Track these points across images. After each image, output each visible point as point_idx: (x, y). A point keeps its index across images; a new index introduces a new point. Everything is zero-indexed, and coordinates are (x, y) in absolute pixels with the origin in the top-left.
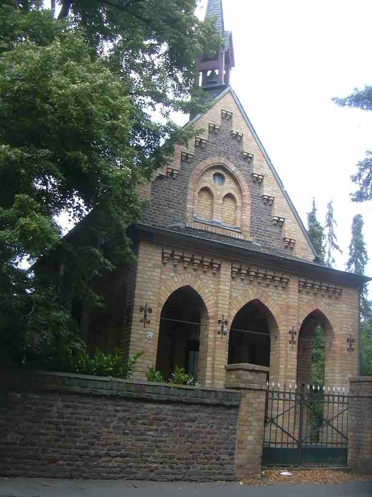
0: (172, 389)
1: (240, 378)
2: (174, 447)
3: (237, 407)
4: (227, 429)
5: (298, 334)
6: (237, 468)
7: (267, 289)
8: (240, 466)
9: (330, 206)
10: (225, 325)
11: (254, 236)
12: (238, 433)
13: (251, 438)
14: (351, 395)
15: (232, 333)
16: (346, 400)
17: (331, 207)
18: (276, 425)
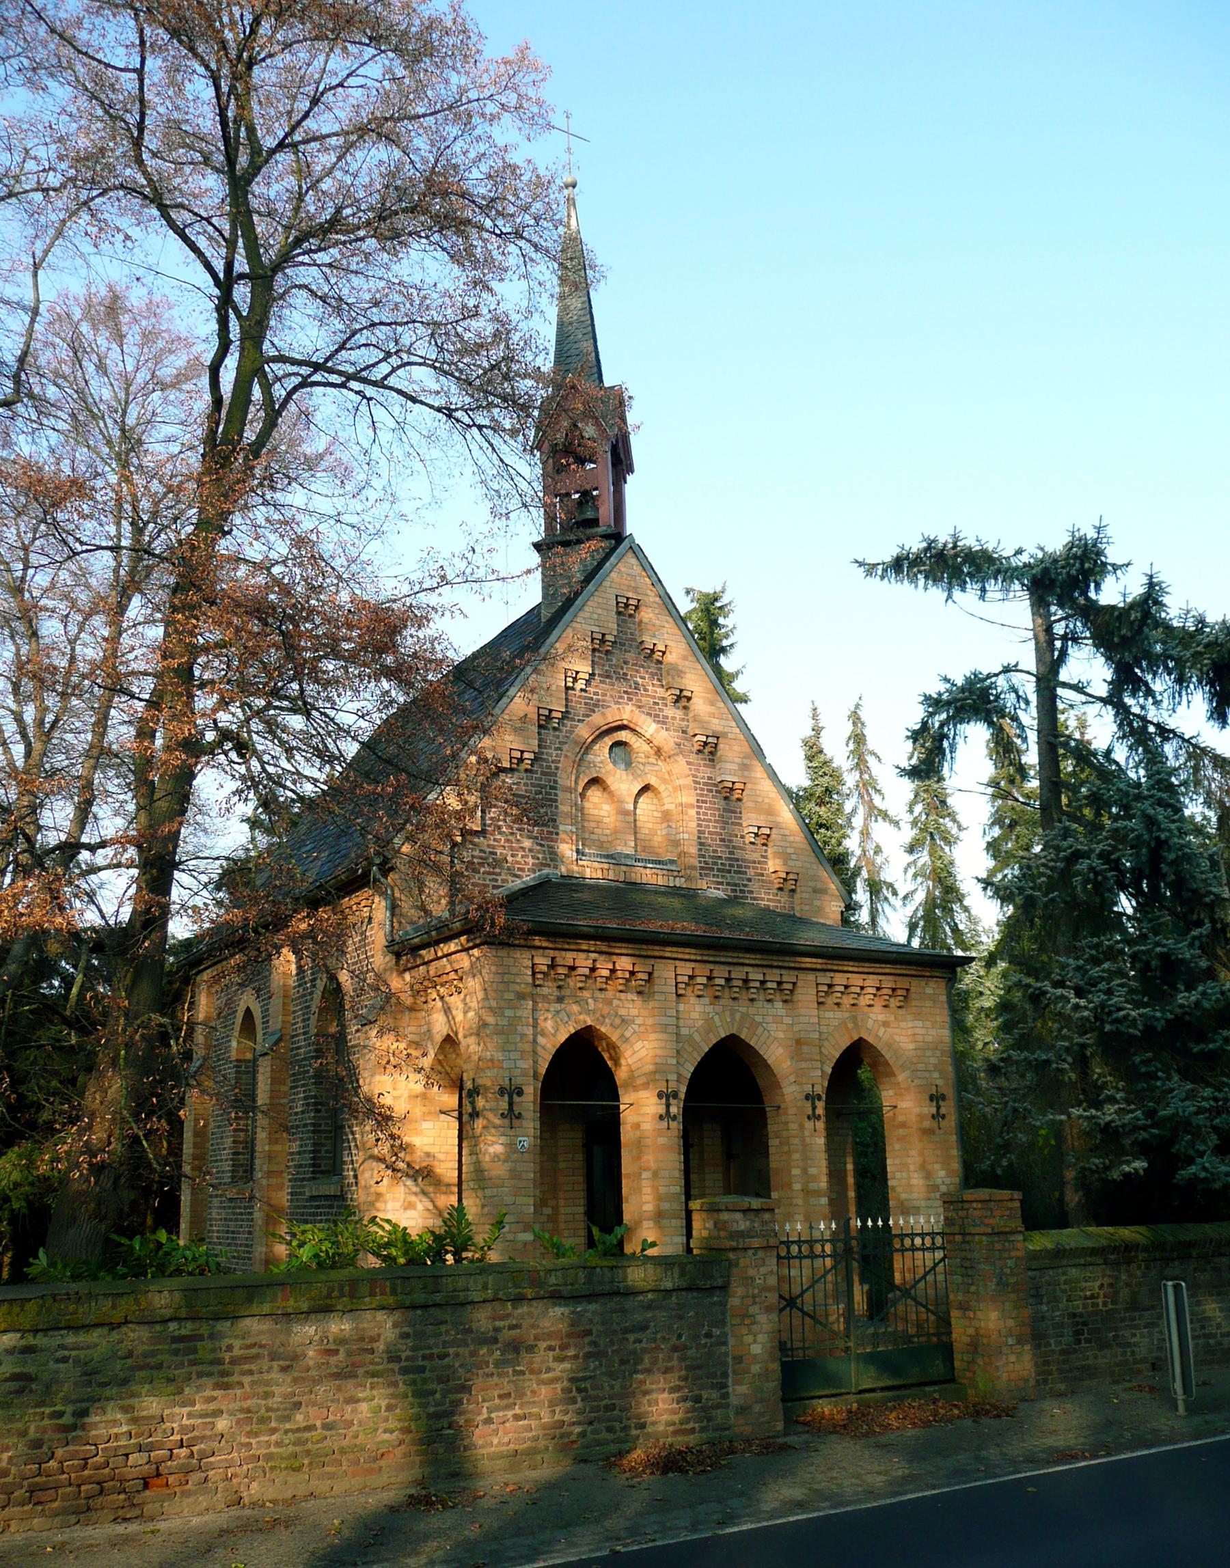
0: (598, 1270)
1: (724, 1229)
2: (612, 1387)
3: (724, 1288)
4: (708, 1335)
5: (824, 1096)
6: (737, 1414)
7: (752, 1011)
8: (742, 1410)
9: (855, 718)
10: (671, 1100)
11: (706, 875)
12: (732, 1341)
13: (756, 1349)
14: (948, 1231)
15: (686, 1111)
16: (939, 1241)
17: (859, 719)
18: (801, 1310)
